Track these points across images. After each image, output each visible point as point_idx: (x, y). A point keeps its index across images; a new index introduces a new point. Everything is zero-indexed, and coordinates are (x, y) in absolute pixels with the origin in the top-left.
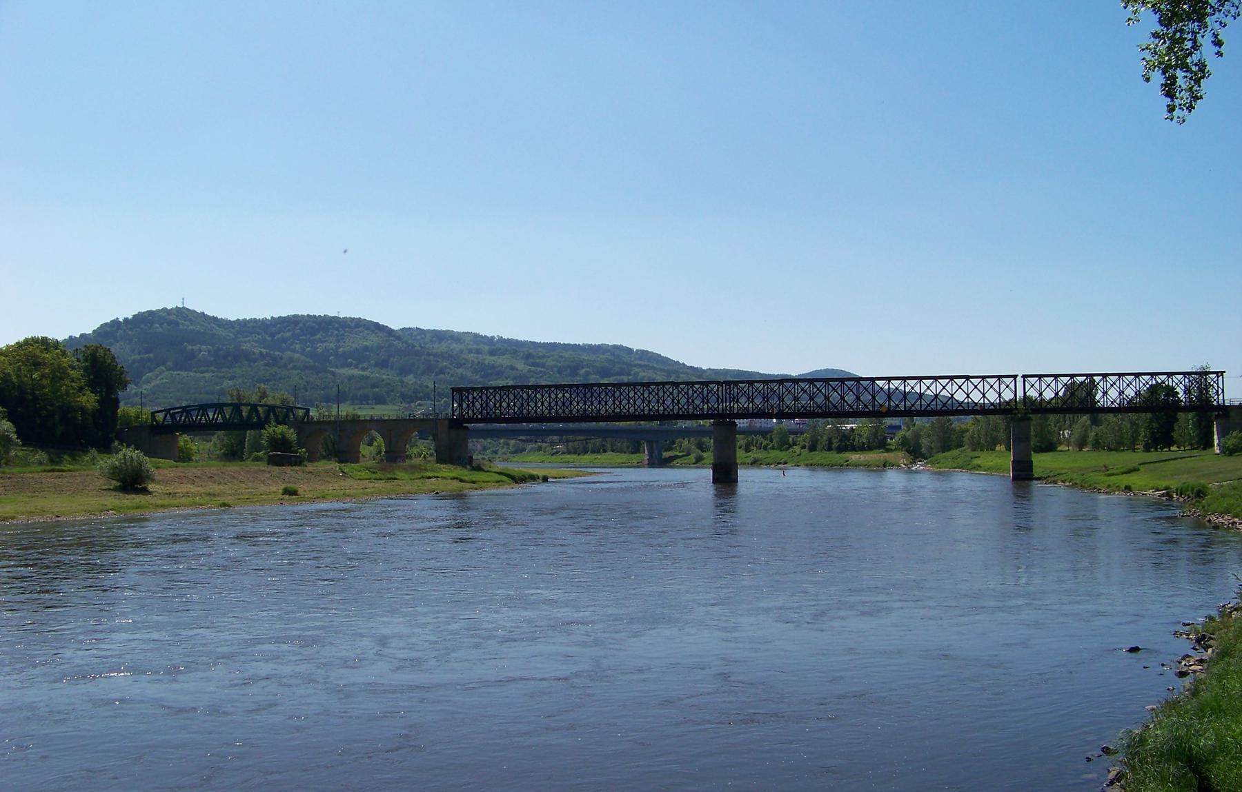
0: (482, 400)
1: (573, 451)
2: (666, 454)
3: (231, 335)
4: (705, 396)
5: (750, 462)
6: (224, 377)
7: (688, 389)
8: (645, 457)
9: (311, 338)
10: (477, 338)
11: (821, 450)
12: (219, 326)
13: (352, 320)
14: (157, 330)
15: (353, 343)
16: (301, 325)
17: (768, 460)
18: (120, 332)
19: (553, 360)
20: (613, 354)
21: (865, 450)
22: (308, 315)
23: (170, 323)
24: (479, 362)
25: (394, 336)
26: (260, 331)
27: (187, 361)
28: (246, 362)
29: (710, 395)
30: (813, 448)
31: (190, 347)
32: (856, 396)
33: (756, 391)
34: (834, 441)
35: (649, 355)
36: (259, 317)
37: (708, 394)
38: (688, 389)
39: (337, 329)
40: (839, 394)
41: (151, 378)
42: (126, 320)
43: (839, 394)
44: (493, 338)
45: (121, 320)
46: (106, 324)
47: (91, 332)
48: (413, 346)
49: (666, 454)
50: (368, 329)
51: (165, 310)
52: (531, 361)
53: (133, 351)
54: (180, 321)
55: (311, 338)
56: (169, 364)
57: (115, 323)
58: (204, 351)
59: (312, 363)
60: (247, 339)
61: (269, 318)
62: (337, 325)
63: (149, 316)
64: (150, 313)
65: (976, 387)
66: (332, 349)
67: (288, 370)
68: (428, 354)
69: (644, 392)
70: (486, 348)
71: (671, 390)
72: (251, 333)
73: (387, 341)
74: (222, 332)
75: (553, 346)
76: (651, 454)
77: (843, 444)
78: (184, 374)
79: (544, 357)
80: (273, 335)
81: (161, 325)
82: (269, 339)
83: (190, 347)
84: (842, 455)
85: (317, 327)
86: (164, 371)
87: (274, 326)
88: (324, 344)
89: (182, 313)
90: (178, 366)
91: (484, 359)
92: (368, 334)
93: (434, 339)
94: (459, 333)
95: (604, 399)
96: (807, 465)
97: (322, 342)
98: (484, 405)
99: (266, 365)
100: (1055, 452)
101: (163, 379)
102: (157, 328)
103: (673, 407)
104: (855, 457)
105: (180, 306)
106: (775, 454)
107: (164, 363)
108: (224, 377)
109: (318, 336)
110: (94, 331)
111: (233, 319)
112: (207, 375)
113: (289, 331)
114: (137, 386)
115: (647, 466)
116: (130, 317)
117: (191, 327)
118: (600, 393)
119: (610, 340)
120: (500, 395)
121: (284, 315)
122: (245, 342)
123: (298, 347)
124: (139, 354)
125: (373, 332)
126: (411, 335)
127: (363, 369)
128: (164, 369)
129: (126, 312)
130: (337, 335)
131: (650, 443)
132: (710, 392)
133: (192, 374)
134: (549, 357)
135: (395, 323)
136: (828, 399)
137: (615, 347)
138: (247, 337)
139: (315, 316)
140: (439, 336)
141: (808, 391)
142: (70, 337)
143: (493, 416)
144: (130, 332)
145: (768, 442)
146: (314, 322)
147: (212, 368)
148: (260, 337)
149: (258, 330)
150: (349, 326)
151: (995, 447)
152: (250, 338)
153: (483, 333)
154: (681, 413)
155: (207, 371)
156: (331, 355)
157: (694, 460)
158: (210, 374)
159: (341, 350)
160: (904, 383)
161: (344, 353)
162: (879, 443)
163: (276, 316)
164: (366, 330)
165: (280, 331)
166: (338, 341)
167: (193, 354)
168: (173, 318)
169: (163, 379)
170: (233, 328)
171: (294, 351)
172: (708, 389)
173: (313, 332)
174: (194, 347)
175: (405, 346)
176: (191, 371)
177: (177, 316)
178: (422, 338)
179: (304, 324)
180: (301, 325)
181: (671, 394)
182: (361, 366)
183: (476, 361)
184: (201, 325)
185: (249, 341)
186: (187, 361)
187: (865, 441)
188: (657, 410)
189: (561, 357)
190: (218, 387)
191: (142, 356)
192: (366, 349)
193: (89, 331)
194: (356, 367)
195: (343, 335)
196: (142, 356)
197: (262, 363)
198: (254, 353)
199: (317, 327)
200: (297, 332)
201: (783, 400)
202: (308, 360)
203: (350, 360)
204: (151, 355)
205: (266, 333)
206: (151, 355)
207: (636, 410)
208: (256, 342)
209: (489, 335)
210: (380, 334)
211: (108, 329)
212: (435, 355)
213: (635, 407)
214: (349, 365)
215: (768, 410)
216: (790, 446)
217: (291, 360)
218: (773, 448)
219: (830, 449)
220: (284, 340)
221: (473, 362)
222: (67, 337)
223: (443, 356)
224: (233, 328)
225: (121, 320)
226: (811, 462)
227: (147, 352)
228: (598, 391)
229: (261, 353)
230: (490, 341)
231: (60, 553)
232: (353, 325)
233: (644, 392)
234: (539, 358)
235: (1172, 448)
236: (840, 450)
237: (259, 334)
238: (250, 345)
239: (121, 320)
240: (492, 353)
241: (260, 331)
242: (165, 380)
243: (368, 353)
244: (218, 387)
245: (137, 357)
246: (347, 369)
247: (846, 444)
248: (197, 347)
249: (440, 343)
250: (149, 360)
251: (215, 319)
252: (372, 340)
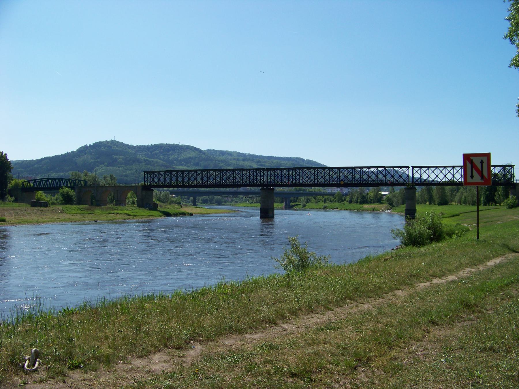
0: (254, 175)
1: (258, 202)
2: (292, 204)
3: (133, 152)
4: (338, 174)
5: (322, 207)
6: (127, 169)
7: (345, 171)
8: (284, 205)
9: (168, 153)
10: (239, 154)
11: (354, 203)
12: (129, 148)
13: (185, 146)
14: (103, 150)
15: (185, 155)
16: (163, 148)
17: (331, 207)
18: (88, 150)
19: (269, 164)
20: (296, 161)
21: (368, 203)
22: (166, 144)
23: (109, 147)
24: (237, 164)
25: (202, 153)
26: (146, 150)
27: (113, 163)
28: (137, 163)
29: (341, 175)
30: (350, 202)
31: (115, 157)
32: (400, 175)
33: (351, 173)
34: (359, 198)
35: (312, 162)
36: (146, 144)
37: (347, 173)
38: (345, 171)
39: (178, 150)
40: (391, 174)
41: (97, 169)
42: (90, 145)
43: (391, 174)
44: (246, 154)
45: (88, 145)
46: (82, 147)
47: (76, 150)
48: (210, 157)
49: (292, 204)
50: (191, 149)
51: (106, 141)
52: (259, 164)
53: (92, 158)
54: (113, 146)
55: (168, 153)
56: (106, 164)
57: (86, 147)
58: (120, 158)
59: (165, 164)
60: (141, 154)
61: (150, 145)
62: (178, 148)
63: (100, 143)
64: (100, 143)
65: (441, 172)
66: (176, 158)
67: (155, 167)
68: (216, 161)
69: (317, 174)
70: (241, 158)
71: (328, 172)
72: (143, 151)
73: (199, 155)
74: (130, 151)
75: (271, 158)
76: (286, 203)
77: (363, 200)
78: (111, 168)
79: (265, 162)
80: (151, 152)
81: (104, 148)
82: (150, 153)
83: (115, 157)
84: (361, 205)
85: (170, 149)
86: (103, 167)
87: (152, 148)
88: (173, 156)
89: (114, 143)
90: (109, 164)
91: (239, 163)
92: (191, 152)
93: (221, 154)
94: (231, 152)
95: (286, 179)
96: (345, 210)
97: (172, 155)
98: (248, 178)
99: (146, 164)
100: (448, 206)
101: (102, 170)
102: (103, 149)
103: (330, 180)
104: (366, 206)
105: (113, 140)
106: (336, 204)
107: (103, 163)
108: (127, 169)
109: (170, 152)
110: (77, 150)
111: (135, 145)
112: (121, 168)
113: (158, 150)
114: (92, 173)
115: (284, 209)
116: (92, 144)
117: (117, 149)
118: (303, 174)
119: (295, 156)
120: (247, 175)
121: (156, 144)
122: (139, 155)
123: (161, 157)
124: (94, 159)
125: (193, 151)
126: (211, 152)
127: (188, 167)
128: (103, 166)
129: (90, 142)
130: (178, 152)
131: (285, 198)
132: (336, 173)
133: (115, 168)
134: (267, 162)
135: (204, 148)
136: (385, 177)
137: (297, 158)
138: (140, 153)
139: (169, 144)
140: (223, 153)
141: (383, 173)
142: (67, 152)
143: (259, 183)
144: (91, 151)
145: (334, 199)
146: (168, 147)
147: (123, 165)
148: (146, 153)
149: (145, 150)
150: (183, 148)
151: (426, 203)
152: (142, 153)
153: (241, 152)
154: (326, 183)
155: (121, 167)
156: (175, 160)
157: (302, 207)
158: (122, 168)
159: (180, 158)
160: (421, 169)
161: (181, 159)
162: (379, 200)
163: (153, 144)
164: (191, 150)
165: (154, 150)
166: (179, 155)
167: (116, 160)
168: (109, 144)
169: (102, 170)
170: (135, 149)
171: (160, 159)
172: (340, 171)
173: (168, 151)
174: (117, 157)
175: (206, 157)
176: (114, 167)
177: (111, 144)
178: (216, 154)
179: (165, 148)
180: (163, 148)
181: (336, 173)
182: (187, 165)
183: (236, 163)
184: (121, 148)
185: (141, 155)
186: (113, 163)
187: (372, 199)
188: (321, 182)
189: (272, 162)
190: (124, 174)
191: (95, 160)
192: (190, 158)
193: (75, 150)
194: (185, 166)
195: (181, 152)
196: (95, 160)
197: (144, 163)
198: (141, 159)
199: (170, 149)
200: (162, 151)
201: (370, 177)
202: (164, 162)
203: (183, 163)
204: (99, 160)
205: (149, 151)
206: (99, 160)
207: (303, 181)
208: (144, 155)
209: (244, 153)
210: (196, 152)
211: (83, 149)
212: (219, 161)
213: (303, 180)
214: (182, 165)
215: (355, 182)
216: (343, 201)
217: (157, 162)
218: (335, 202)
219: (357, 202)
220: (156, 154)
221: (234, 164)
222: (66, 152)
223: (222, 161)
224: (135, 149)
225: (88, 145)
226: (346, 208)
227: (97, 158)
228: (306, 171)
229: (144, 159)
230: (244, 155)
231: (197, 214)
232: (185, 148)
233: (317, 174)
234: (263, 162)
235: (497, 205)
236: (361, 203)
237: (145, 151)
238: (141, 156)
239: (88, 145)
240: (244, 160)
241: (146, 150)
242: (103, 170)
243: (190, 160)
244: (124, 174)
245: (93, 161)
246: (181, 166)
247: (364, 200)
248: (118, 157)
249: (223, 156)
250: (98, 162)
251: (127, 145)
252: (193, 154)
